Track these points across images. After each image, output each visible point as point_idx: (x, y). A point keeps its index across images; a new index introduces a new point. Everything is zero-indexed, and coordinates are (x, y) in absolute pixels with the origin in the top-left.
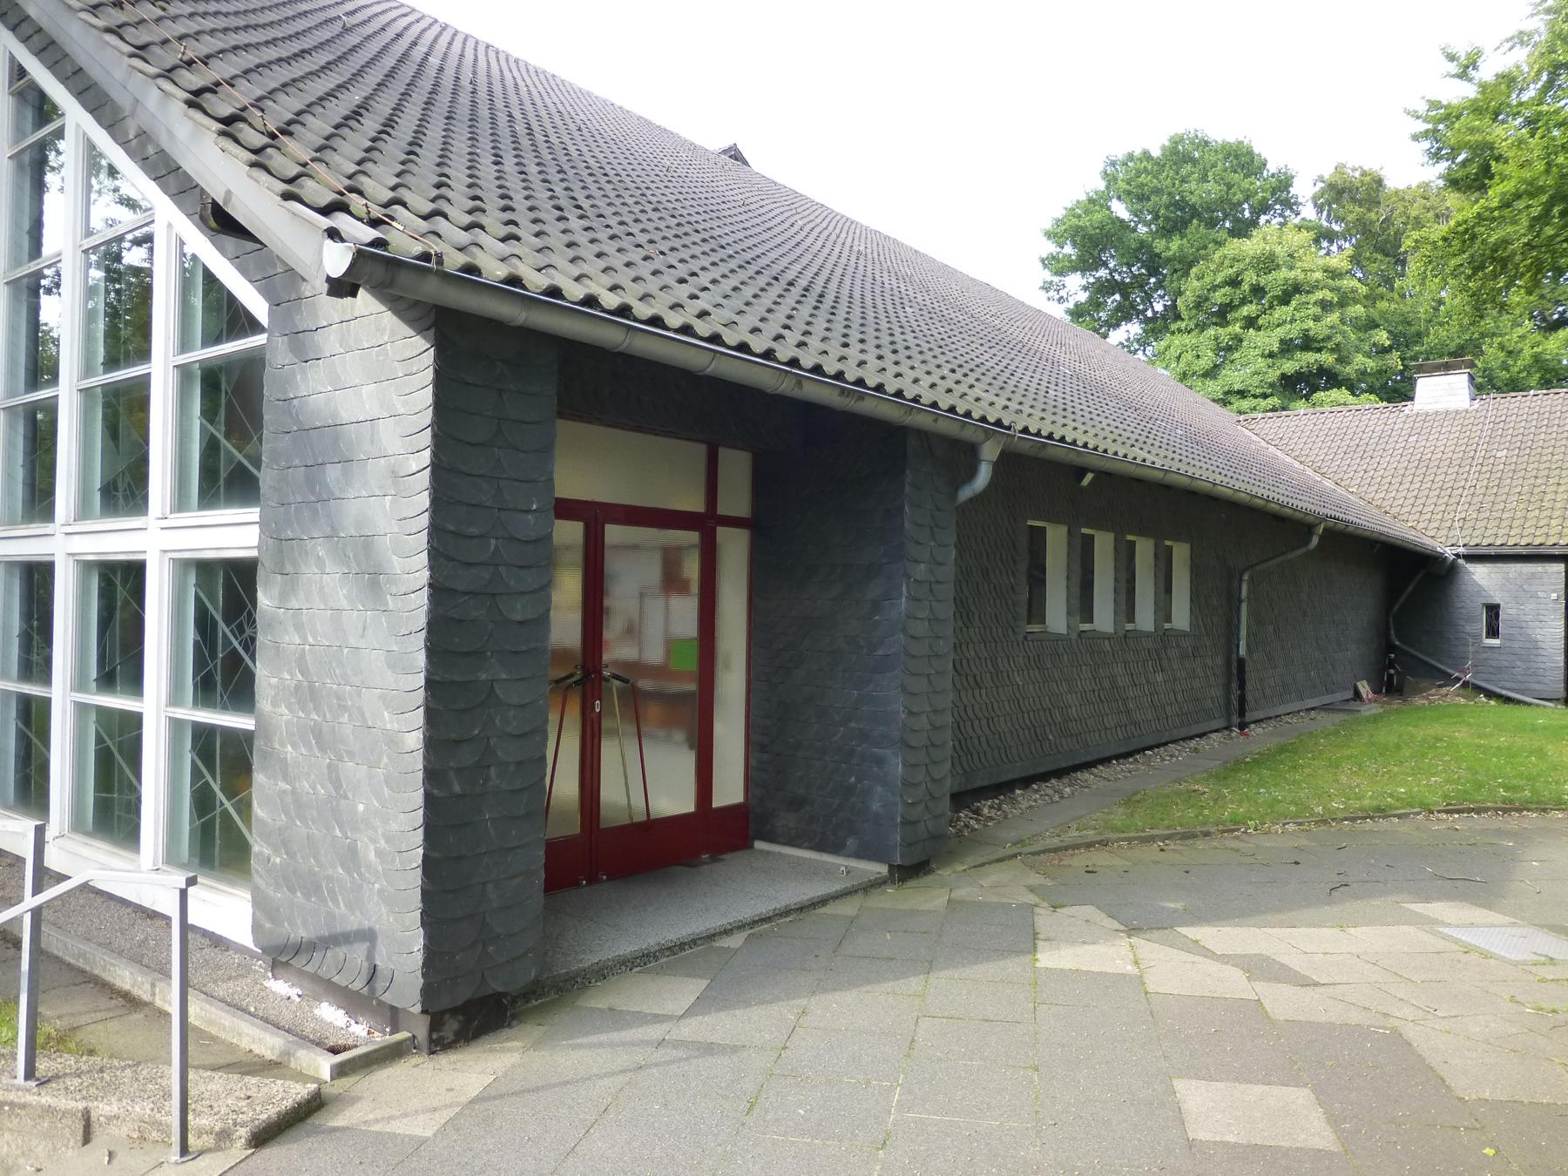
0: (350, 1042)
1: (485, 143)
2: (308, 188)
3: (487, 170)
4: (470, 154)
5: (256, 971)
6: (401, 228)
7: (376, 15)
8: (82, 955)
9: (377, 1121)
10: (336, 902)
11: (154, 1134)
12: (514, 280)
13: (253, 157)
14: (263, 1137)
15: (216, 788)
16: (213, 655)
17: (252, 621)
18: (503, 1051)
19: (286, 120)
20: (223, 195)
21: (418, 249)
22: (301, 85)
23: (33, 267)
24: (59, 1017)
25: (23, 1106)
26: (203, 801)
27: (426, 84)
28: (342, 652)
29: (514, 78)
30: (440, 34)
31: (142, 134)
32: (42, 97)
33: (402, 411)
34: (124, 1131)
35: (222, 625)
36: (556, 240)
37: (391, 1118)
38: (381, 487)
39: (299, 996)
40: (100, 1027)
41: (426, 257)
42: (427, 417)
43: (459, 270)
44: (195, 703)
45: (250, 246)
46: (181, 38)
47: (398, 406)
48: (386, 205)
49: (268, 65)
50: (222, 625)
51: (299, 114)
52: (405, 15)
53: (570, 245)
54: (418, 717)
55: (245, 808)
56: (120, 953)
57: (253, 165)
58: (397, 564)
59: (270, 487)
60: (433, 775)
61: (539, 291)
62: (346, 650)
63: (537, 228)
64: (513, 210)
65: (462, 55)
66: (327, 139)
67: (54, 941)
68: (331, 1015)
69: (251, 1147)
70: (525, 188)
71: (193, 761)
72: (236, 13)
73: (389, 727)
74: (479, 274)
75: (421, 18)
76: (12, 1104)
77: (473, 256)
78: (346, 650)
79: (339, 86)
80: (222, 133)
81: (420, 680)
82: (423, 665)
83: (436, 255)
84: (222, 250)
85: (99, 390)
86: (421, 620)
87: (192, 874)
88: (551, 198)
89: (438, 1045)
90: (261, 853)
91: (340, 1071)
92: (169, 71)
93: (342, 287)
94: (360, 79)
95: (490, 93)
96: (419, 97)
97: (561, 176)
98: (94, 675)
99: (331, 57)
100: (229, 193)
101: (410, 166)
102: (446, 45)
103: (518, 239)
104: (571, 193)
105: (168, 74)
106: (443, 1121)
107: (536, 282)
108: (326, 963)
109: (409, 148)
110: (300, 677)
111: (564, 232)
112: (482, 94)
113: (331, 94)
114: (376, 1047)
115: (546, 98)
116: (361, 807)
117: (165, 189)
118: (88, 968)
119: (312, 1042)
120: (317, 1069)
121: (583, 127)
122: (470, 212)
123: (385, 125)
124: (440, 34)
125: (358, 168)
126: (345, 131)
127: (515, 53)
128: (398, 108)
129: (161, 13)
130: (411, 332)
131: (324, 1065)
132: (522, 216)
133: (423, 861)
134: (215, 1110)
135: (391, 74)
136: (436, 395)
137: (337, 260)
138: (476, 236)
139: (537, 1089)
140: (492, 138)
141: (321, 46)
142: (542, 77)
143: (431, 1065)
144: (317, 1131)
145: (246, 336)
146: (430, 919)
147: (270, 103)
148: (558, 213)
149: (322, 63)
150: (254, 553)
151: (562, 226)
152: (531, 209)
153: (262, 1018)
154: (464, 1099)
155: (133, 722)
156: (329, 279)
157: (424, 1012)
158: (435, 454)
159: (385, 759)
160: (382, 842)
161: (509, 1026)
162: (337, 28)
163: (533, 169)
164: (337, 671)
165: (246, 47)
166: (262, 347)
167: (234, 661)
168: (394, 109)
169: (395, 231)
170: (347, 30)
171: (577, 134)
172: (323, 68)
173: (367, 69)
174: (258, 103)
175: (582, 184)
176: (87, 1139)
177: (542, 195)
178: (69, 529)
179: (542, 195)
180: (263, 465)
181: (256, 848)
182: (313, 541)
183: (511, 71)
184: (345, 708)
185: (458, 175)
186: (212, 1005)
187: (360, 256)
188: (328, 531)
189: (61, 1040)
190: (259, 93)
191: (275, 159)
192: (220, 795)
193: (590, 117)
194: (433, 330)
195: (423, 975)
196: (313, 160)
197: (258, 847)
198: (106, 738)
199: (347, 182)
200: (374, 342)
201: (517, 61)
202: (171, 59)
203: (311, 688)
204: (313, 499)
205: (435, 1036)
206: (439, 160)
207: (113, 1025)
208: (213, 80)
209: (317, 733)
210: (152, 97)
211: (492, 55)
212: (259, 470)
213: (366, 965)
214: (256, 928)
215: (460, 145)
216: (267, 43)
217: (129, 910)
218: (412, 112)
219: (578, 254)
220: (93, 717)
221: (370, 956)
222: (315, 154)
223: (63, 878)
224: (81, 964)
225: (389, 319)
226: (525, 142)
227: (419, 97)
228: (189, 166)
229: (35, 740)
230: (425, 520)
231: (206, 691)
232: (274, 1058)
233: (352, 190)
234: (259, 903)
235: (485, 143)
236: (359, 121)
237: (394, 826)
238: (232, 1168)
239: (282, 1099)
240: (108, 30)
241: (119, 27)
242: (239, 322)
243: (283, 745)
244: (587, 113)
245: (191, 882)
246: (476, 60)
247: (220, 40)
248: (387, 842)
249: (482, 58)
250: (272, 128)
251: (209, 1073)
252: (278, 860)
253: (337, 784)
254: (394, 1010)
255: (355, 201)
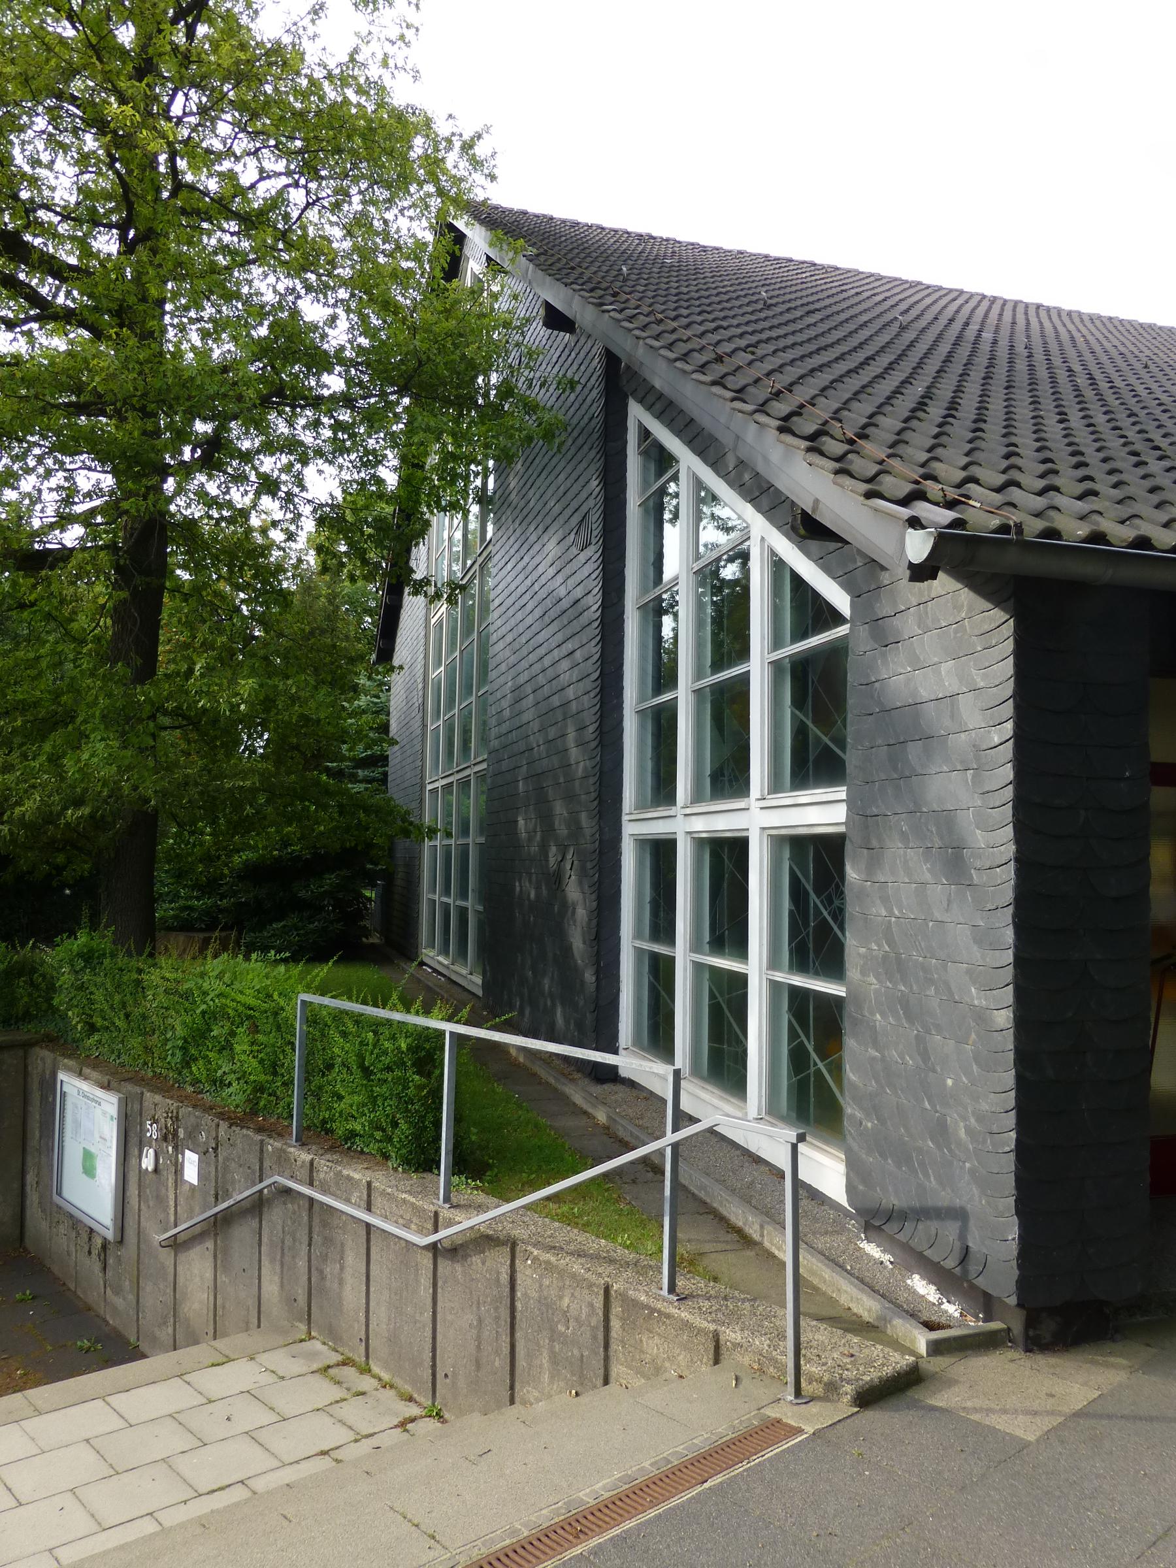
0: (943, 1320)
1: (1047, 404)
2: (888, 483)
3: (1053, 430)
4: (1033, 418)
5: (849, 1230)
6: (978, 505)
7: (928, 307)
8: (703, 1188)
9: (976, 1410)
10: (927, 1175)
11: (771, 1369)
12: (1098, 537)
13: (837, 465)
14: (869, 1398)
15: (810, 1048)
16: (806, 925)
17: (840, 894)
18: (1107, 1365)
19: (861, 424)
20: (811, 504)
21: (995, 522)
22: (869, 390)
23: (657, 592)
24: (689, 1241)
25: (668, 1316)
26: (798, 1059)
27: (982, 360)
28: (927, 925)
29: (1069, 332)
30: (990, 308)
31: (741, 463)
32: (661, 449)
33: (982, 684)
34: (746, 1360)
35: (813, 896)
36: (1137, 488)
37: (989, 1411)
38: (962, 762)
39: (891, 1263)
40: (721, 1256)
41: (1004, 529)
42: (1009, 689)
43: (1038, 536)
44: (791, 968)
45: (833, 546)
46: (768, 374)
47: (978, 680)
48: (959, 486)
49: (839, 379)
50: (813, 896)
51: (871, 416)
52: (954, 300)
53: (1152, 490)
54: (1008, 994)
55: (837, 1069)
56: (733, 1191)
57: (837, 472)
58: (980, 838)
59: (856, 767)
60: (1025, 1059)
61: (1124, 544)
62: (931, 924)
63: (1114, 479)
64: (1087, 465)
65: (1014, 323)
66: (898, 434)
67: (692, 1178)
68: (923, 1287)
69: (856, 1406)
70: (1095, 441)
71: (790, 1022)
72: (809, 340)
73: (976, 1002)
74: (1060, 538)
75: (970, 298)
76: (653, 1310)
77: (1051, 519)
78: (931, 924)
79: (903, 382)
80: (809, 450)
81: (1009, 957)
82: (1011, 941)
83: (1016, 525)
84: (808, 554)
85: (708, 689)
86: (1009, 895)
87: (801, 1131)
88: (1125, 445)
89: (1035, 1343)
90: (852, 1116)
91: (936, 1348)
92: (762, 405)
93: (922, 572)
94: (920, 371)
95: (1047, 352)
96: (977, 375)
97: (1133, 419)
98: (707, 939)
99: (892, 357)
100: (817, 501)
101: (978, 443)
102: (996, 317)
103: (1095, 493)
104: (1146, 436)
105: (762, 409)
106: (1046, 1429)
107: (1121, 534)
108: (919, 1234)
109: (974, 426)
110: (887, 948)
111: (1144, 477)
112: (1039, 357)
113: (897, 392)
114: (971, 1332)
115: (1105, 343)
116: (950, 1082)
117: (758, 509)
118: (708, 1201)
119: (907, 1312)
120: (913, 1341)
121: (1150, 363)
122: (1042, 476)
123: (948, 409)
124: (990, 308)
125: (929, 455)
126: (914, 423)
127: (1067, 306)
128: (959, 390)
129: (752, 357)
130: (990, 606)
131: (921, 1341)
132: (1097, 469)
133: (1016, 1146)
134: (824, 1360)
135: (948, 359)
136: (1017, 665)
137: (918, 546)
138: (1052, 499)
139: (1151, 1419)
140: (1054, 397)
141: (882, 350)
142: (1098, 323)
143: (1028, 1364)
144: (916, 1405)
145: (829, 629)
146: (1025, 1207)
147: (846, 413)
148: (1135, 459)
149: (885, 365)
150: (842, 829)
151: (1141, 471)
152: (1105, 460)
153: (857, 1278)
154: (1066, 1410)
155: (739, 982)
156: (911, 566)
157: (1020, 1305)
158: (1017, 726)
159: (973, 1036)
160: (973, 1120)
161: (1113, 1340)
162: (895, 328)
163: (1100, 419)
164: (923, 944)
165: (820, 368)
166: (845, 637)
167: (824, 931)
168: (954, 392)
169: (971, 509)
170: (903, 328)
171: (1143, 373)
172: (886, 369)
173: (926, 360)
174: (836, 416)
175: (1157, 423)
176: (717, 1361)
177: (1114, 443)
178: (688, 811)
179: (1114, 443)
180: (849, 747)
181: (849, 1110)
182: (897, 817)
183: (1065, 325)
184: (931, 982)
185: (1026, 441)
186: (813, 1256)
187: (942, 541)
188: (911, 807)
189: (692, 1263)
190: (836, 405)
191: (856, 463)
192: (814, 1055)
193: (1156, 351)
194: (1012, 600)
195: (1018, 1265)
196: (889, 456)
197: (850, 1109)
198: (718, 995)
199: (922, 471)
200: (952, 620)
201: (1069, 313)
202: (761, 394)
203: (898, 960)
204: (896, 776)
205: (1031, 1333)
206: (1004, 431)
207: (731, 1257)
208: (797, 403)
209: (904, 1002)
210: (750, 432)
211: (1043, 314)
212: (845, 752)
213: (958, 1244)
214: (850, 1189)
215: (1023, 411)
216: (837, 359)
217: (738, 1152)
218: (973, 389)
219: (1163, 498)
220: (707, 975)
221: (962, 1236)
222: (890, 451)
223: (693, 1120)
224: (702, 1195)
225: (966, 596)
226: (1089, 394)
227: (977, 375)
228: (782, 484)
229: (663, 993)
230: (1009, 793)
231: (801, 961)
232: (868, 1319)
233: (927, 477)
234: (853, 1166)
235: (1047, 404)
236: (925, 411)
237: (984, 1106)
238: (839, 1421)
239: (883, 1365)
240: (714, 383)
241: (722, 378)
242: (827, 616)
243: (873, 1014)
244: (1152, 347)
245: (801, 1138)
246: (1028, 323)
247: (799, 367)
248: (977, 1120)
249: (1034, 321)
250: (850, 434)
251: (814, 1323)
252: (869, 1125)
253: (924, 1054)
254: (986, 1295)
255: (932, 488)
